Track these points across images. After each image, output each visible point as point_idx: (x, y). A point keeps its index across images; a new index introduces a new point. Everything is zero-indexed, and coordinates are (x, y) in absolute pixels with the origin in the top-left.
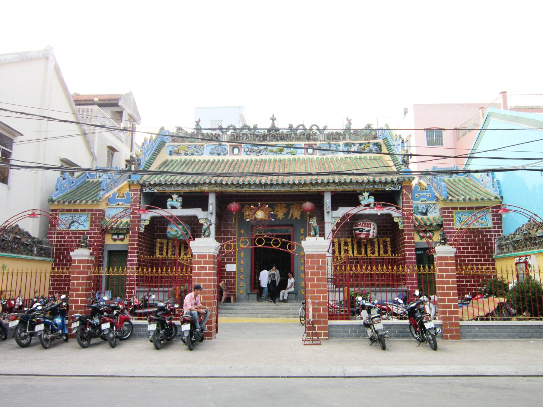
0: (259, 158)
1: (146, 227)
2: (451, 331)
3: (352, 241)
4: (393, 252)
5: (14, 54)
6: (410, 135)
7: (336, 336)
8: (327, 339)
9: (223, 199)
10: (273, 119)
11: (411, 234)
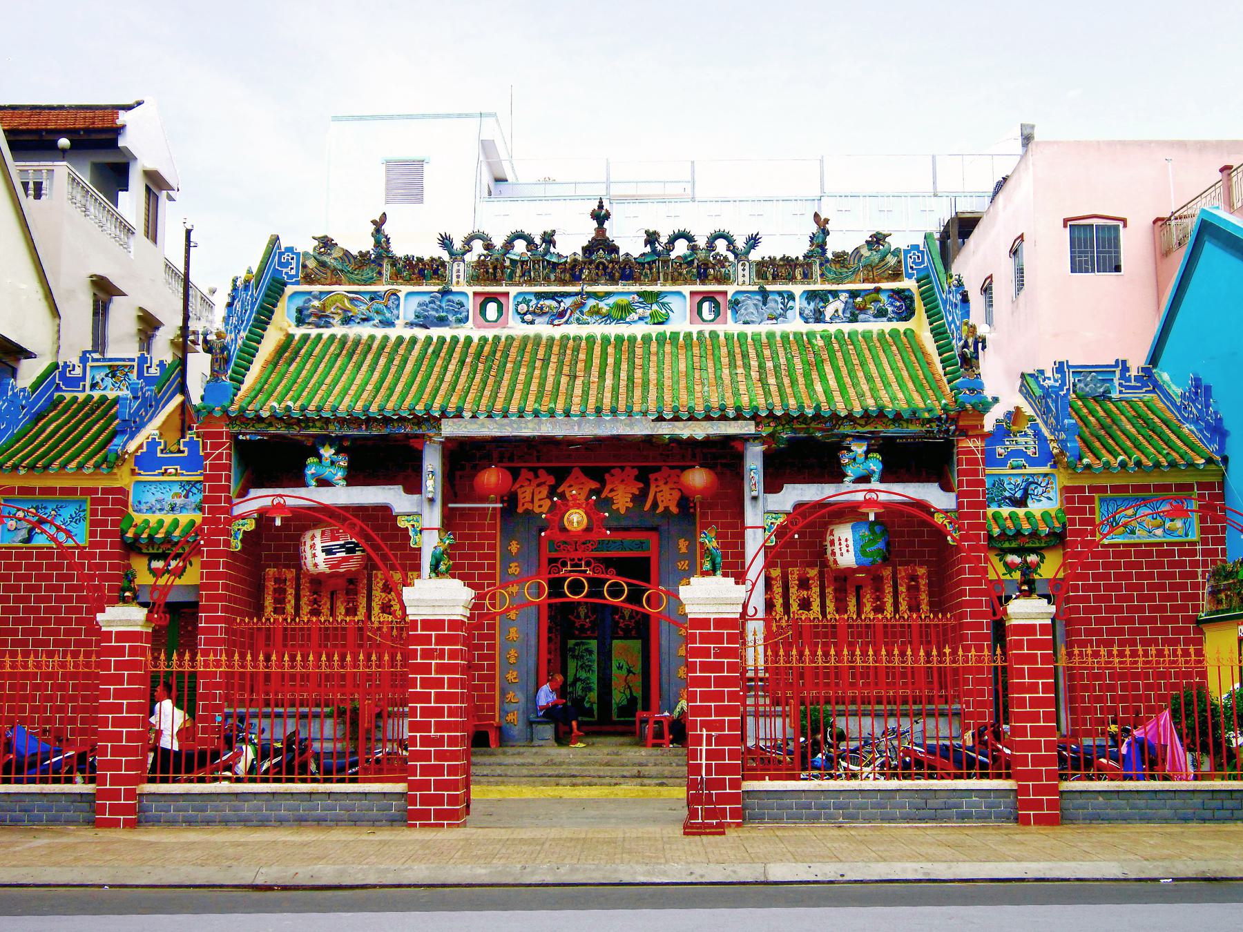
0: (558, 332)
2: (1037, 805)
4: (936, 606)
6: (1021, 236)
7: (761, 818)
8: (738, 825)
9: (465, 457)
10: (600, 216)
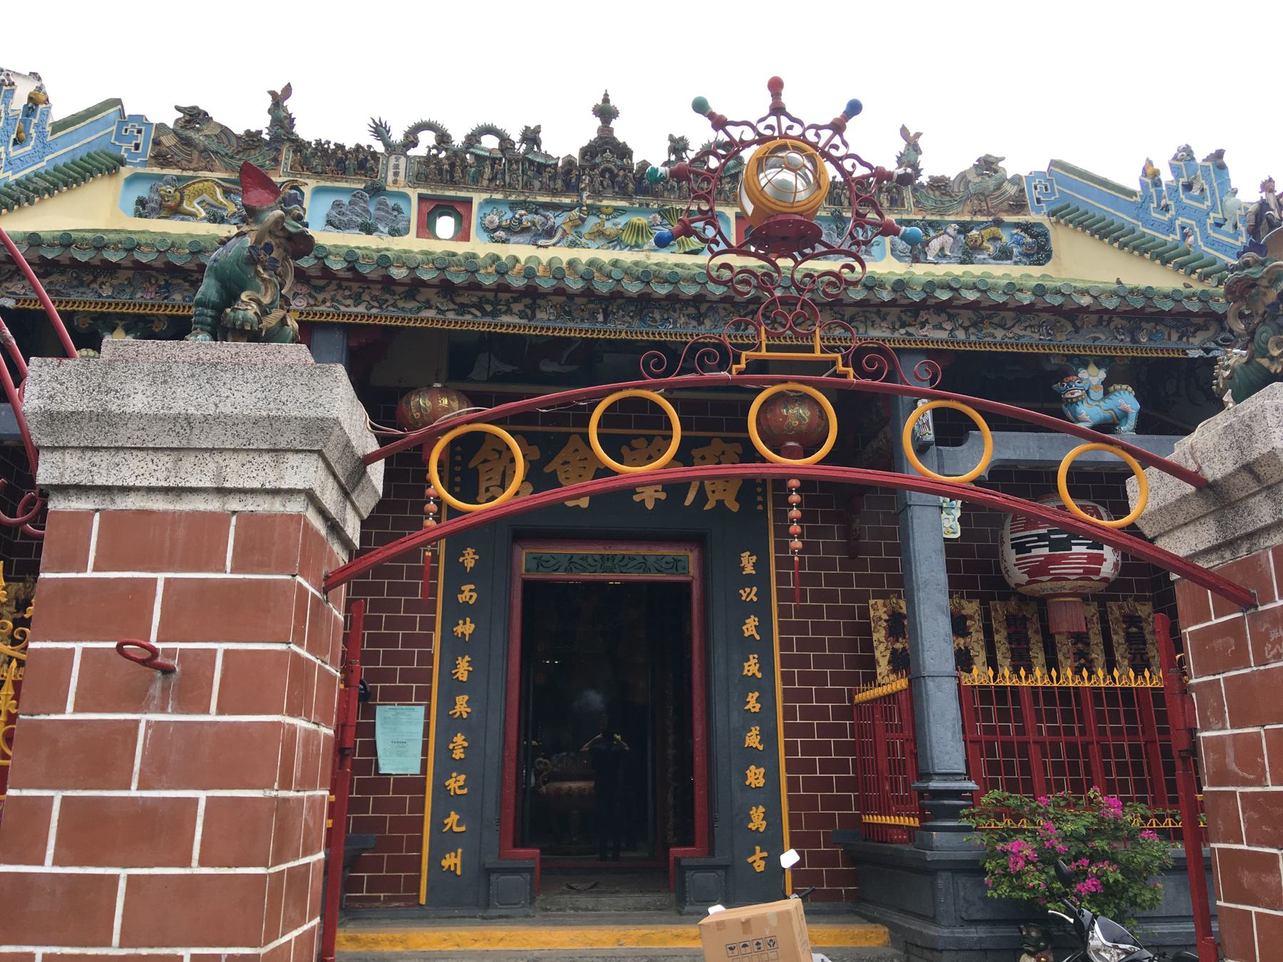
3: (986, 616)
5: (492, 918)
10: (606, 112)
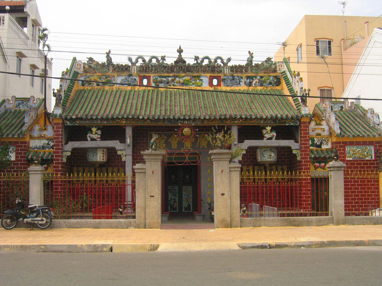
1: (68, 158)
10: (180, 51)
11: (307, 165)
